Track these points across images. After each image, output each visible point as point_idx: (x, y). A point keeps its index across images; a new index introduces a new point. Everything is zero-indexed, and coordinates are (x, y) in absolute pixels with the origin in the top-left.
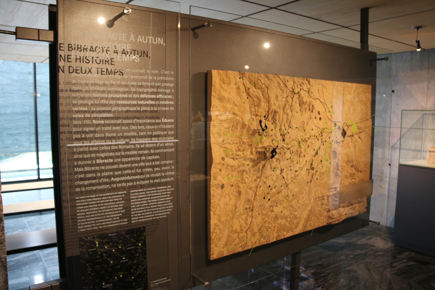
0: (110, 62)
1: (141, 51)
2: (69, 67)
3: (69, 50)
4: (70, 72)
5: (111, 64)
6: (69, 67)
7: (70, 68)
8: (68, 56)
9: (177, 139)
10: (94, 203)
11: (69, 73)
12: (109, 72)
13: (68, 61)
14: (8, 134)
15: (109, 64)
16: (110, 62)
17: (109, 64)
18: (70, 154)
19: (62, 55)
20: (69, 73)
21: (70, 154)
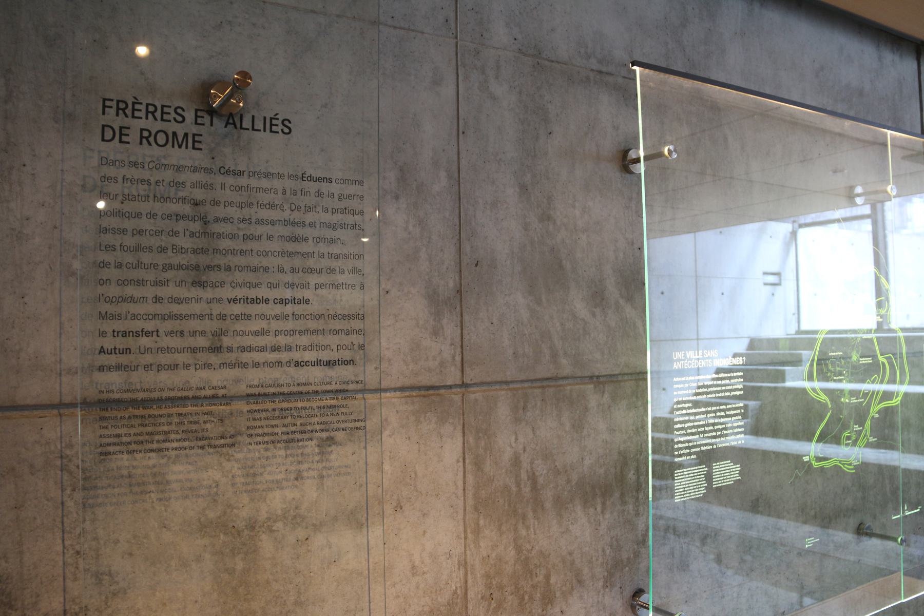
0: (158, 114)
1: (265, 118)
2: (104, 126)
3: (196, 123)
4: (106, 138)
5: (162, 120)
6: (104, 126)
7: (106, 129)
8: (194, 135)
9: (835, 435)
10: (688, 492)
11: (103, 140)
12: (180, 141)
13: (194, 148)
14: (515, 442)
15: (156, 119)
16: (158, 114)
17: (156, 119)
18: (230, 303)
19: (178, 134)
20: (103, 140)
21: (230, 303)
